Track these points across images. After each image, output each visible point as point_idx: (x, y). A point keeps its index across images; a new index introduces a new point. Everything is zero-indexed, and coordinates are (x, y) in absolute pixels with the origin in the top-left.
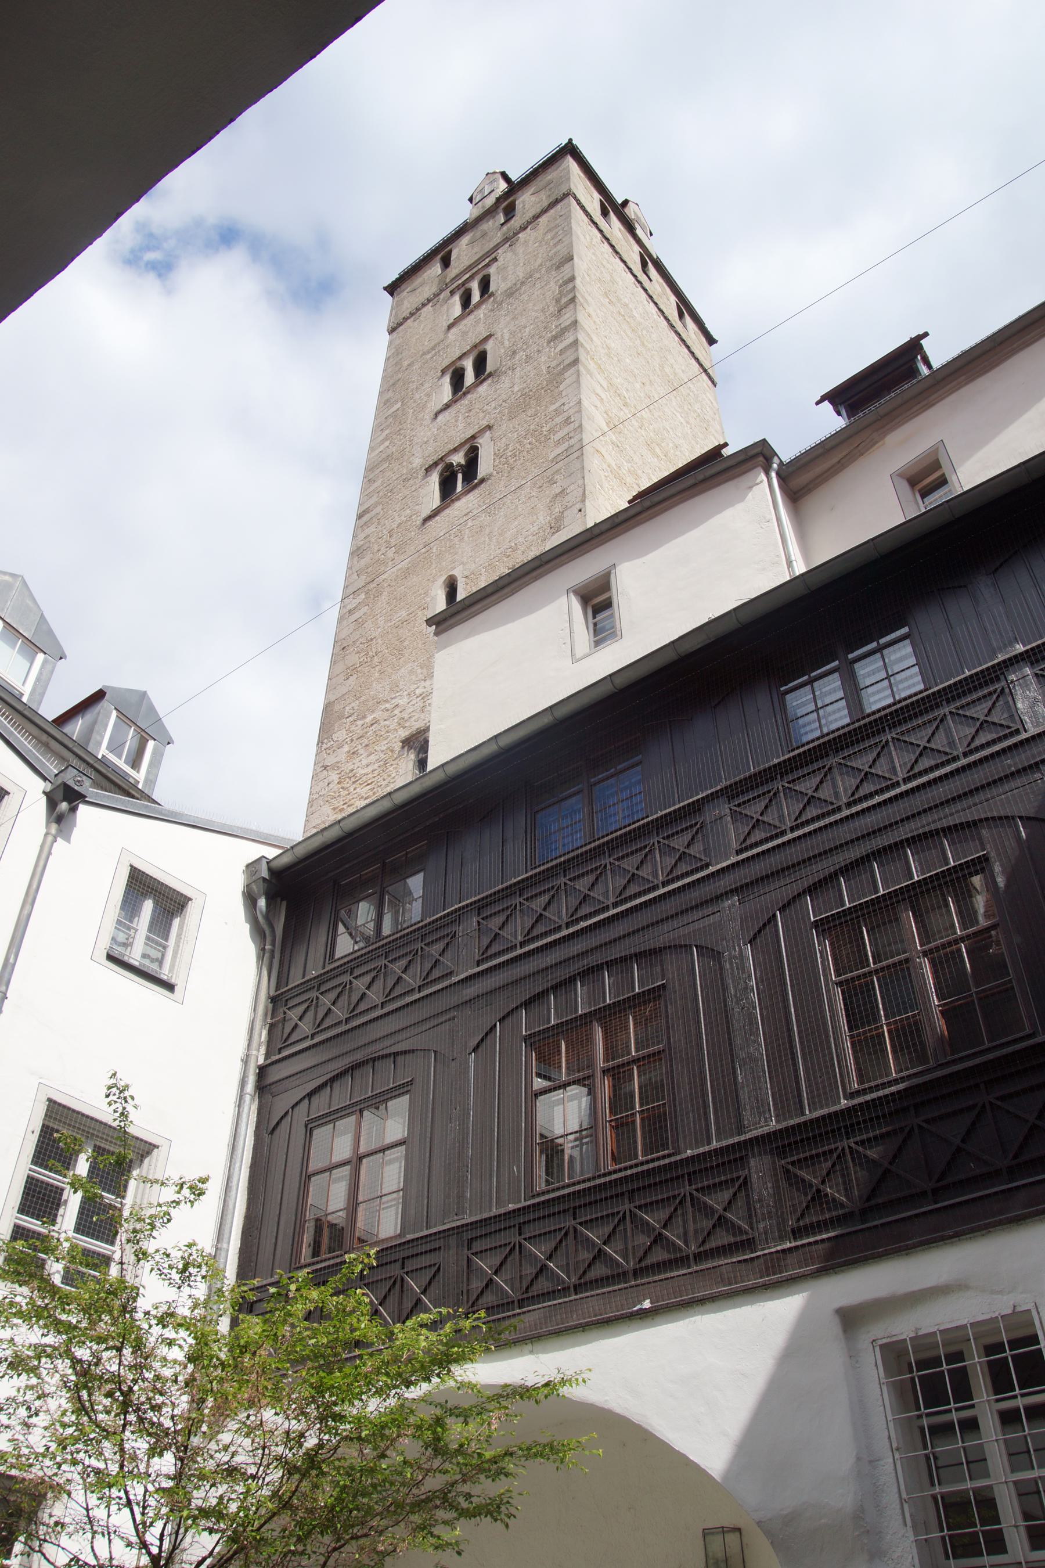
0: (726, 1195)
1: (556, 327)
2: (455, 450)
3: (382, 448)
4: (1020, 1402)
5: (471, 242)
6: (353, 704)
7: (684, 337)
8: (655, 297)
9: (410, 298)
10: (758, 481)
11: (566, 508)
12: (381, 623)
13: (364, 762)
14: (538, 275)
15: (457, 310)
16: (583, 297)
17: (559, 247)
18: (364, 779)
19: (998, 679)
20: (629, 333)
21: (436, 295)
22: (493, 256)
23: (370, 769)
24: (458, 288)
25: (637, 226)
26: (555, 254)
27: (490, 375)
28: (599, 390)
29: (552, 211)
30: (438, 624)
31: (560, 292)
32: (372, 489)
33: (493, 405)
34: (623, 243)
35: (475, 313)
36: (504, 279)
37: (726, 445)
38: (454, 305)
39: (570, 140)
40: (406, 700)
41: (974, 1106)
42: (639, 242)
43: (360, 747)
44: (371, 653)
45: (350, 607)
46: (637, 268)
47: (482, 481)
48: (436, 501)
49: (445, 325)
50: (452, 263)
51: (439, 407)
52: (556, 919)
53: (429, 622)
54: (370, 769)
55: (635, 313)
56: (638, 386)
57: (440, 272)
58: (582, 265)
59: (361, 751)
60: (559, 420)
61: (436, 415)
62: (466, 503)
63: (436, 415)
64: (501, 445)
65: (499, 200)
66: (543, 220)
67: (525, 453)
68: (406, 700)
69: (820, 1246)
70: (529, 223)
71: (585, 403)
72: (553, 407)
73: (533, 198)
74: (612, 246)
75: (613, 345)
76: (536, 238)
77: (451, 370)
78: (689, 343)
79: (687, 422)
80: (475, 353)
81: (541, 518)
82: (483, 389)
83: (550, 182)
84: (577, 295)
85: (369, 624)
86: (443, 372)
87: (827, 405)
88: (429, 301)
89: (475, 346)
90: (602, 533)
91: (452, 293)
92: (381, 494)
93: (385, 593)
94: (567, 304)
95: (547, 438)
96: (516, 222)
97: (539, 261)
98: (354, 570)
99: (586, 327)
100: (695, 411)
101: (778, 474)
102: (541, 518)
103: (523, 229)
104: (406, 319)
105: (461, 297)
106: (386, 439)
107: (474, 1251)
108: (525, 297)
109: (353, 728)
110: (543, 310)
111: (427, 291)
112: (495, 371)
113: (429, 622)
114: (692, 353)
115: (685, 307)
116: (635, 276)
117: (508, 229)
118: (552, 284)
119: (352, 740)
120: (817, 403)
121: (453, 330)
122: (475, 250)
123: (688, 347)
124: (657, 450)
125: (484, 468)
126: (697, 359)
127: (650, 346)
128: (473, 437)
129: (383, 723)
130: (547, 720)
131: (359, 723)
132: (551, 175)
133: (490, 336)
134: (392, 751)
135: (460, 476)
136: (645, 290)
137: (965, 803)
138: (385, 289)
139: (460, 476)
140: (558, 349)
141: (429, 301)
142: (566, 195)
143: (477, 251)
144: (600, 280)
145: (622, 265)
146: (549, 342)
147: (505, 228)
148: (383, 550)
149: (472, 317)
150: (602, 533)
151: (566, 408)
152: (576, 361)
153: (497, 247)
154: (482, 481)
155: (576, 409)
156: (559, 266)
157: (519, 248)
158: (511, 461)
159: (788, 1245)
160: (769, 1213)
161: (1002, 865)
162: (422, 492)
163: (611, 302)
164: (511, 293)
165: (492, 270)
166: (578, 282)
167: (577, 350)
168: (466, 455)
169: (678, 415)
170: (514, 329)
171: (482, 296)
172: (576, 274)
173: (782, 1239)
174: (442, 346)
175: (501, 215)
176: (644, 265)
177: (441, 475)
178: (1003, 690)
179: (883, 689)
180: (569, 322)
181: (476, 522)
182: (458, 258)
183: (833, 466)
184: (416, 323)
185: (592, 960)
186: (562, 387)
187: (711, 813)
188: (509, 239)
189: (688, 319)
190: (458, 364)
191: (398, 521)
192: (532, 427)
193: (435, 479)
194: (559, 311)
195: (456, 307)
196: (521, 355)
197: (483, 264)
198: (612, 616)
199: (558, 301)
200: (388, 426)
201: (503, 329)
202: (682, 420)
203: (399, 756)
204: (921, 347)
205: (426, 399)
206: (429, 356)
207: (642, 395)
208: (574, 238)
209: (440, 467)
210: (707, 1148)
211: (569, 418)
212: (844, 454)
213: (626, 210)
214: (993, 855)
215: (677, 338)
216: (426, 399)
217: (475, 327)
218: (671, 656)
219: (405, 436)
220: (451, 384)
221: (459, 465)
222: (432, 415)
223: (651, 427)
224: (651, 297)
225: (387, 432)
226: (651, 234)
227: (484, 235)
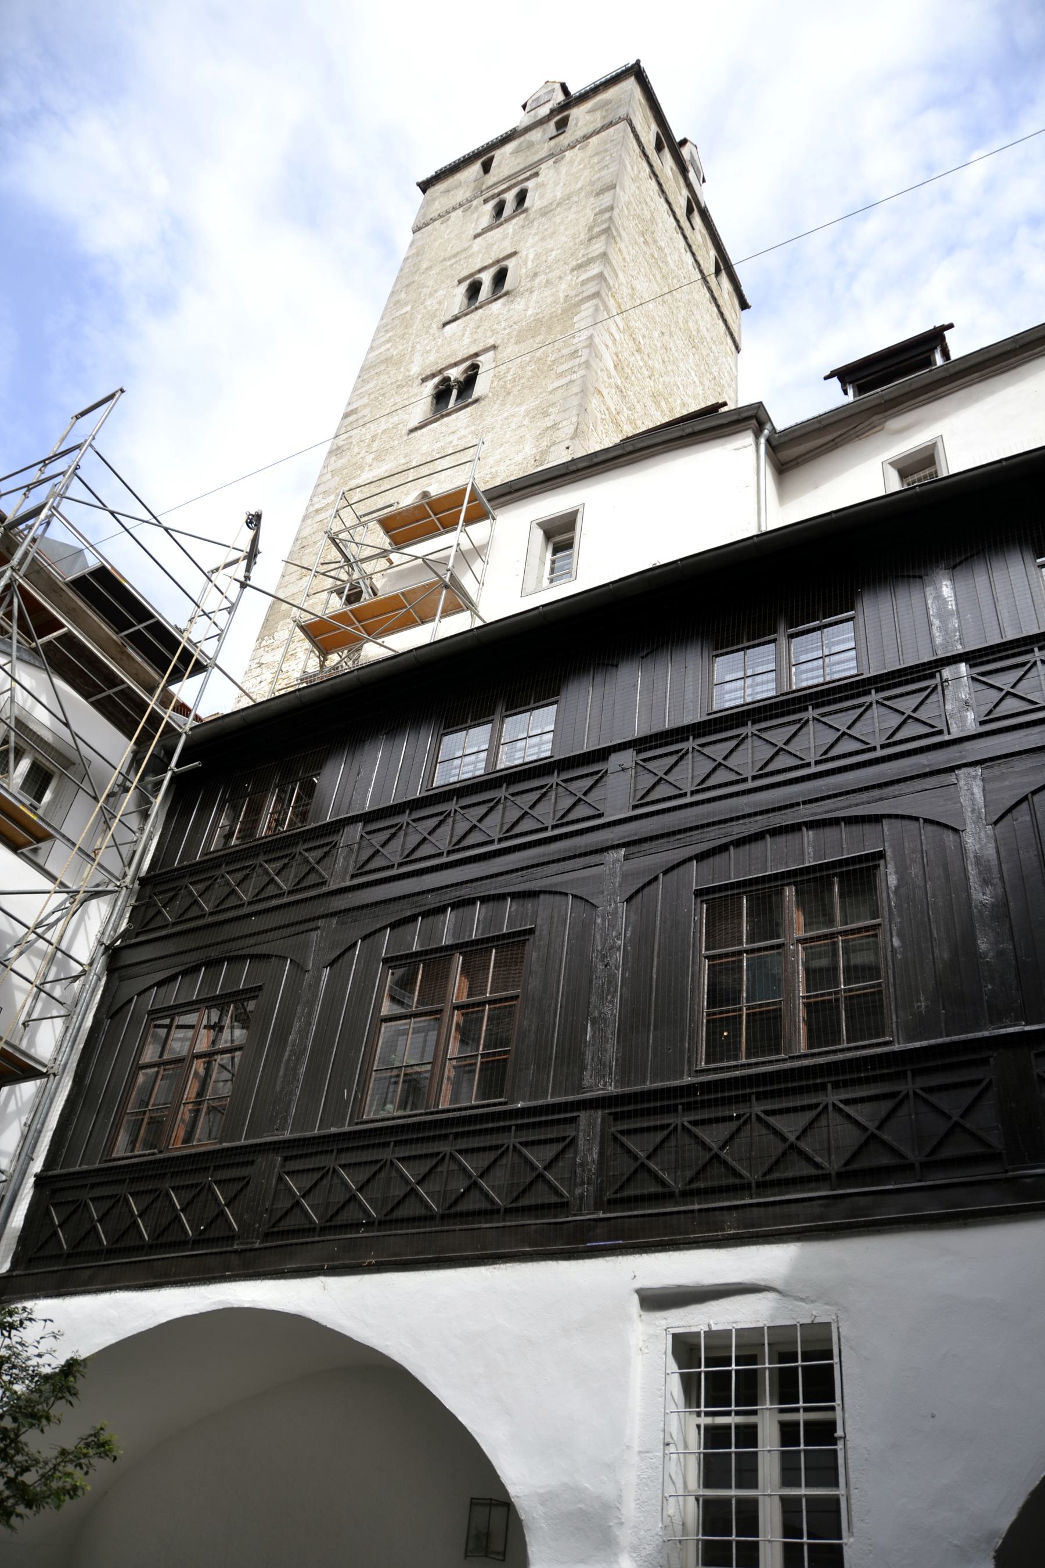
1: (583, 256)
2: (456, 364)
4: (801, 1417)
5: (517, 151)
7: (716, 294)
8: (694, 248)
9: (443, 195)
11: (554, 444)
14: (575, 199)
16: (617, 230)
17: (603, 173)
19: (932, 676)
20: (658, 279)
24: (493, 197)
25: (691, 169)
26: (599, 179)
29: (603, 134)
31: (594, 220)
32: (363, 390)
33: (503, 325)
34: (672, 183)
35: (505, 226)
36: (541, 197)
37: (725, 404)
39: (638, 62)
41: (817, 1105)
42: (689, 186)
45: (317, 506)
46: (682, 213)
47: (476, 401)
49: (472, 233)
55: (669, 259)
56: (656, 334)
63: (444, 325)
65: (553, 112)
66: (594, 140)
73: (588, 117)
74: (660, 184)
75: (639, 287)
77: (468, 282)
78: (721, 302)
79: (701, 383)
83: (608, 102)
87: (835, 380)
88: (461, 205)
89: (498, 261)
90: (578, 470)
91: (486, 201)
92: (372, 396)
95: (550, 368)
96: (565, 139)
97: (579, 185)
98: (329, 469)
100: (711, 373)
103: (571, 147)
104: (433, 220)
106: (388, 341)
107: (286, 1169)
108: (558, 219)
114: (722, 314)
115: (724, 265)
116: (677, 221)
118: (588, 211)
120: (826, 378)
121: (479, 240)
123: (718, 306)
124: (663, 404)
125: (480, 387)
126: (725, 321)
128: (477, 355)
135: (455, 392)
136: (685, 238)
138: (419, 185)
139: (455, 392)
140: (581, 279)
141: (461, 205)
145: (666, 206)
146: (573, 270)
147: (553, 142)
150: (578, 470)
153: (541, 161)
154: (476, 401)
157: (563, 167)
160: (589, 1179)
161: (896, 866)
163: (645, 242)
164: (545, 212)
165: (530, 185)
173: (597, 1209)
176: (690, 211)
177: (437, 387)
178: (935, 688)
179: (817, 669)
184: (443, 227)
185: (465, 892)
186: (576, 319)
187: (616, 760)
188: (556, 156)
189: (723, 275)
190: (477, 276)
194: (590, 240)
196: (541, 278)
198: (570, 556)
199: (590, 229)
200: (393, 328)
201: (529, 250)
202: (696, 379)
204: (943, 338)
205: (437, 306)
206: (448, 263)
207: (659, 344)
209: (436, 380)
211: (576, 351)
212: (840, 433)
214: (889, 853)
215: (708, 295)
219: (408, 342)
223: (661, 379)
224: (690, 246)
225: (390, 334)
226: (704, 181)
227: (531, 145)
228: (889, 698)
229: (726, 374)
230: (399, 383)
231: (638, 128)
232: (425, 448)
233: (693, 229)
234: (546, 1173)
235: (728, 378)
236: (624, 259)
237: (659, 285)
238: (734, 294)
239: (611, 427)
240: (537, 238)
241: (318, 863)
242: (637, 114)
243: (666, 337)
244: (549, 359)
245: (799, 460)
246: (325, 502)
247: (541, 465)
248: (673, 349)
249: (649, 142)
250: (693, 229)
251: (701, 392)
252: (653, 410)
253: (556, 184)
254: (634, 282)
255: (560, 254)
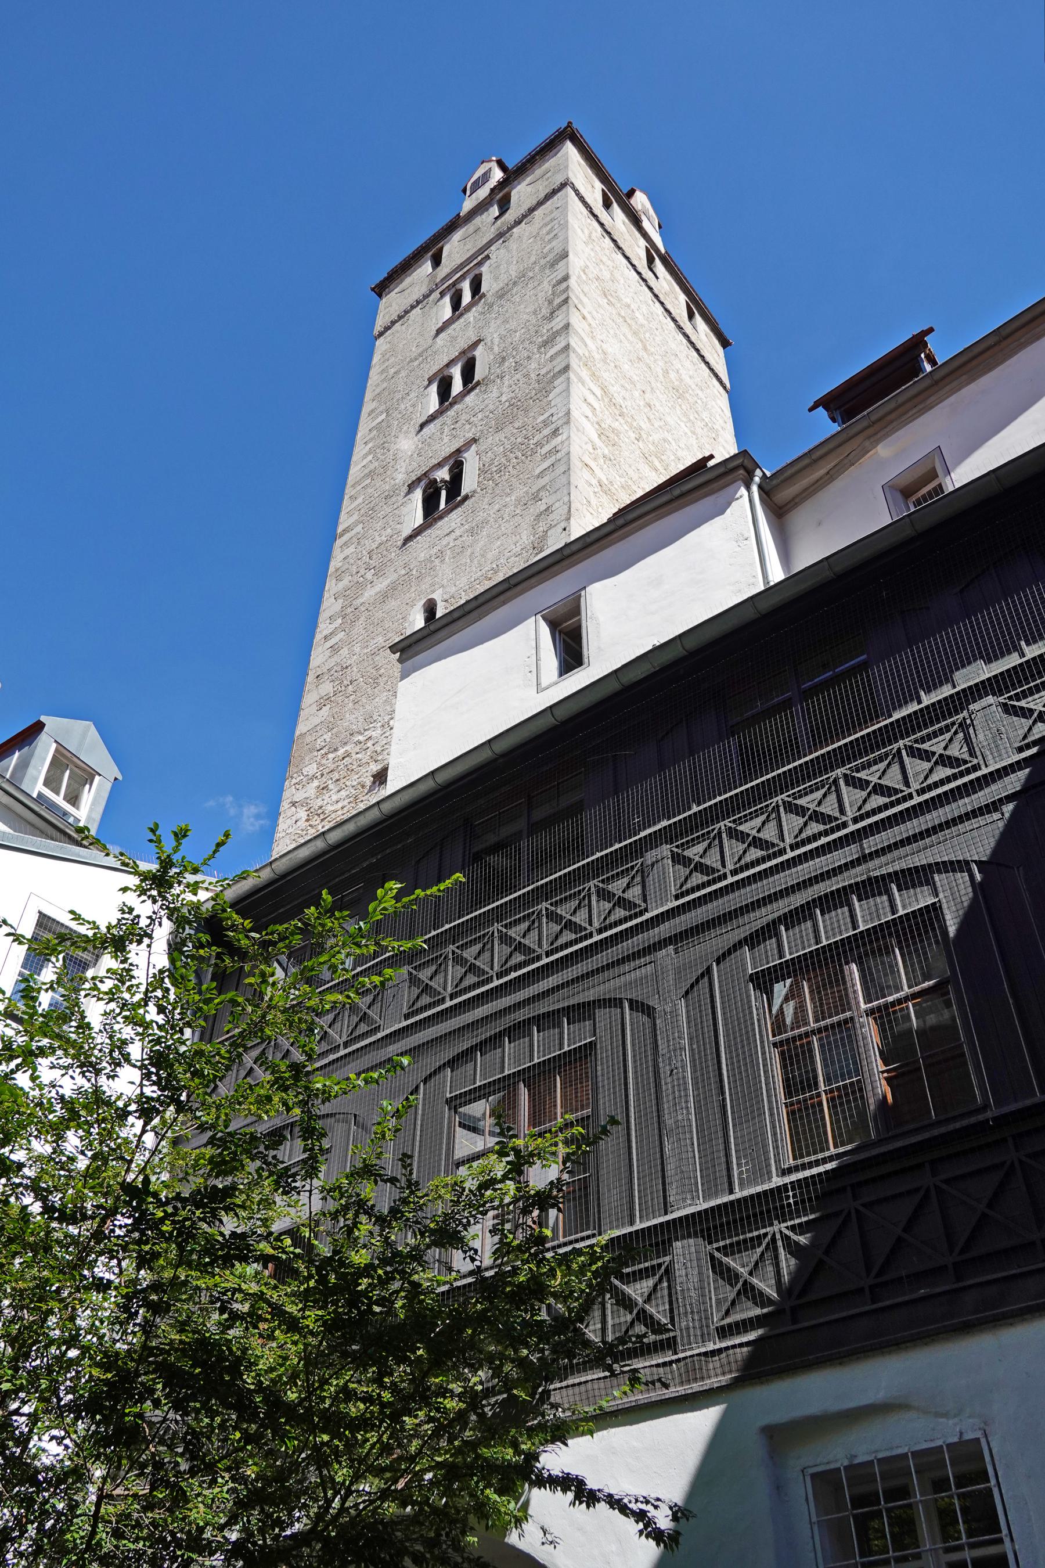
0: (648, 1284)
1: (548, 331)
2: (440, 465)
3: (365, 462)
6: (325, 736)
7: (693, 339)
10: (738, 496)
11: (551, 527)
12: (357, 649)
13: (334, 798)
15: (447, 312)
16: (578, 297)
17: (554, 243)
18: (333, 816)
20: (629, 337)
21: (426, 296)
22: (486, 253)
23: (340, 805)
25: (643, 218)
27: (478, 383)
28: (591, 399)
30: (402, 651)
32: (353, 506)
33: (480, 416)
34: (627, 236)
37: (711, 457)
38: (444, 307)
40: (379, 731)
43: (330, 782)
44: (345, 682)
46: (642, 264)
48: (419, 519)
50: (443, 261)
51: (424, 419)
52: (487, 969)
53: (393, 649)
54: (340, 805)
55: (637, 314)
56: (637, 394)
57: (430, 270)
58: (576, 262)
59: (331, 787)
60: (546, 432)
61: (422, 426)
62: (453, 521)
63: (422, 426)
64: (486, 459)
67: (510, 468)
68: (379, 731)
69: (745, 1349)
70: (524, 216)
71: (575, 414)
72: (542, 418)
73: (529, 189)
74: (614, 241)
75: (610, 350)
76: (531, 233)
78: (699, 346)
79: (694, 433)
80: (464, 360)
81: (524, 537)
82: (469, 399)
84: (571, 295)
85: (345, 652)
86: (430, 381)
88: (418, 302)
91: (442, 294)
92: (362, 511)
93: (363, 618)
94: (560, 306)
95: (534, 453)
96: (510, 216)
97: (533, 259)
99: (580, 331)
101: (760, 487)
102: (524, 537)
103: (518, 223)
105: (451, 299)
106: (369, 452)
109: (324, 761)
110: (535, 312)
111: (417, 293)
112: (483, 380)
113: (393, 649)
114: (702, 357)
116: (639, 273)
117: (502, 223)
119: (322, 775)
120: (811, 410)
122: (468, 247)
123: (697, 350)
125: (468, 485)
126: (707, 364)
127: (653, 350)
129: (354, 756)
130: (486, 754)
131: (331, 756)
132: (551, 163)
133: (479, 341)
134: (363, 786)
135: (444, 493)
136: (650, 289)
137: (889, 856)
139: (444, 493)
140: (549, 355)
141: (418, 302)
142: (563, 185)
143: (470, 248)
144: (598, 278)
145: (625, 261)
147: (499, 222)
148: (362, 572)
149: (462, 320)
151: (555, 418)
152: (567, 368)
155: (565, 420)
156: (553, 264)
157: (513, 244)
158: (496, 477)
159: (711, 1347)
162: (404, 510)
164: (501, 295)
165: (484, 269)
166: (572, 282)
167: (568, 356)
168: (450, 470)
169: (682, 425)
170: (504, 333)
171: (473, 297)
172: (571, 273)
174: (430, 352)
175: (496, 207)
176: (650, 261)
177: (424, 492)
180: (561, 325)
181: (458, 542)
182: (449, 256)
183: (821, 478)
184: (404, 327)
185: (521, 1015)
186: (551, 396)
189: (698, 318)
190: (446, 373)
191: (378, 540)
192: (519, 440)
193: (418, 495)
194: (552, 313)
195: (446, 311)
196: (510, 362)
197: (475, 262)
199: (550, 302)
201: (493, 333)
202: (686, 430)
203: (369, 791)
205: (411, 410)
206: (416, 363)
207: (642, 403)
208: (570, 233)
209: (423, 484)
210: (629, 1229)
212: (833, 464)
213: (632, 201)
215: (685, 341)
216: (411, 410)
217: (463, 333)
218: (614, 686)
220: (439, 394)
221: (443, 481)
222: (417, 428)
224: (656, 296)
225: (370, 445)
228: (923, 740)
229: (718, 417)
230: (386, 493)
231: (582, 191)
232: (422, 555)
233: (657, 278)
234: (647, 1307)
235: (721, 421)
236: (590, 325)
237: (631, 343)
238: (712, 335)
239: (604, 499)
240: (499, 322)
241: (431, 979)
242: (578, 176)
243: (648, 395)
244: (532, 442)
245: (797, 500)
246: (333, 626)
247: (541, 551)
248: (657, 404)
249: (596, 200)
250: (657, 278)
251: (694, 442)
252: (646, 470)
253: (509, 263)
254: (604, 346)
255: (524, 333)
